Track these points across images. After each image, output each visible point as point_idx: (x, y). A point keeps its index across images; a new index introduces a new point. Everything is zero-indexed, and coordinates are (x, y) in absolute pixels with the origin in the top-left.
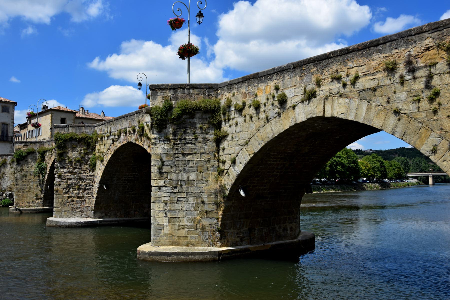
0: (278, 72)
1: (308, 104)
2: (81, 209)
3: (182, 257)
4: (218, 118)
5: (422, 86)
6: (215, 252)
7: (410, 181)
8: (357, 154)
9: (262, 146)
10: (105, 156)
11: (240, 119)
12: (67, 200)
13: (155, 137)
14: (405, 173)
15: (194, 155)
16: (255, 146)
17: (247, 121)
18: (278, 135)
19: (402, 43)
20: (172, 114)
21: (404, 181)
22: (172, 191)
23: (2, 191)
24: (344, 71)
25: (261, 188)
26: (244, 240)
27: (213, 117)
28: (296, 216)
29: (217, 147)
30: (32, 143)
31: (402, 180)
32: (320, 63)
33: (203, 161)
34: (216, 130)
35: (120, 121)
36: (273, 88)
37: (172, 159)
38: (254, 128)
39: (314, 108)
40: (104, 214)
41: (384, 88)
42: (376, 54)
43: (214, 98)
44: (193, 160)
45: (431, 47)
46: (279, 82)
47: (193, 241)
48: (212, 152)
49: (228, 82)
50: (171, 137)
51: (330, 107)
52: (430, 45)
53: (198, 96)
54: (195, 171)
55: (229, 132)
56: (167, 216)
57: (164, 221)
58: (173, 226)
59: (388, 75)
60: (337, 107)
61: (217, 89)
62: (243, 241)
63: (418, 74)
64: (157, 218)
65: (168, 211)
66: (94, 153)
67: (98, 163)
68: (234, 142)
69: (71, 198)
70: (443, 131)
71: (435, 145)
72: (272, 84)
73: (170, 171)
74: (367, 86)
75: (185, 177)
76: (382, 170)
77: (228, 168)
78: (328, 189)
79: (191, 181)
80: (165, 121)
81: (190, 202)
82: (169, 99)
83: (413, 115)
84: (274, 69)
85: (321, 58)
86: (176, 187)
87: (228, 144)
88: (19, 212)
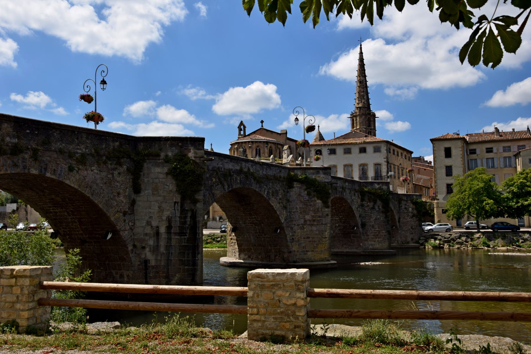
40: (247, 256)
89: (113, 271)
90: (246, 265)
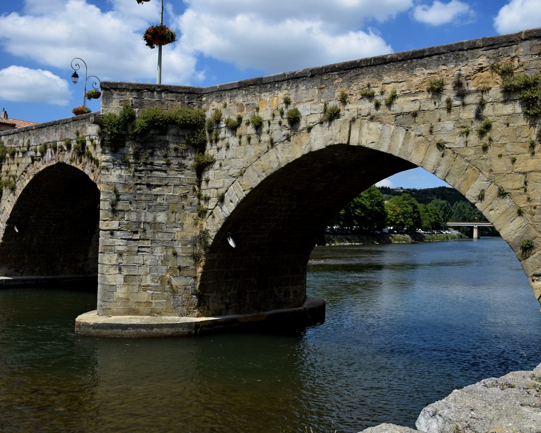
0: (289, 79)
1: (329, 127)
3: (143, 330)
4: (201, 137)
5: (472, 115)
7: (450, 233)
8: (383, 193)
9: (263, 179)
10: (17, 182)
11: (233, 141)
13: (107, 158)
14: (444, 222)
15: (165, 187)
16: (252, 179)
17: (242, 144)
18: (286, 166)
19: (451, 59)
20: (133, 127)
21: (442, 233)
22: (131, 237)
24: (378, 87)
26: (231, 308)
27: (194, 135)
28: (302, 276)
29: (197, 177)
31: (440, 232)
32: (347, 73)
34: (198, 153)
35: (45, 130)
36: (282, 101)
37: (131, 191)
38: (253, 154)
39: (337, 132)
40: (13, 270)
41: (427, 114)
42: (419, 69)
43: (196, 108)
44: (162, 194)
45: (485, 67)
46: (290, 93)
47: (159, 308)
48: (191, 184)
49: (218, 87)
50: (131, 160)
51: (358, 132)
52: (484, 66)
53: (173, 104)
54: (165, 210)
55: (216, 157)
56: (122, 273)
57: (117, 280)
58: (131, 287)
59: (433, 97)
61: (202, 96)
63: (469, 99)
64: (106, 276)
65: (124, 265)
67: (6, 192)
68: (224, 172)
70: (492, 173)
71: (483, 190)
72: (281, 95)
73: (128, 209)
74: (406, 110)
75: (150, 219)
76: (415, 217)
77: (212, 208)
78: (341, 240)
79: (160, 223)
80: (123, 136)
81: (156, 254)
82: (130, 105)
83: (459, 150)
84: (284, 75)
86: (136, 232)
87: (213, 174)
90: (18, 283)
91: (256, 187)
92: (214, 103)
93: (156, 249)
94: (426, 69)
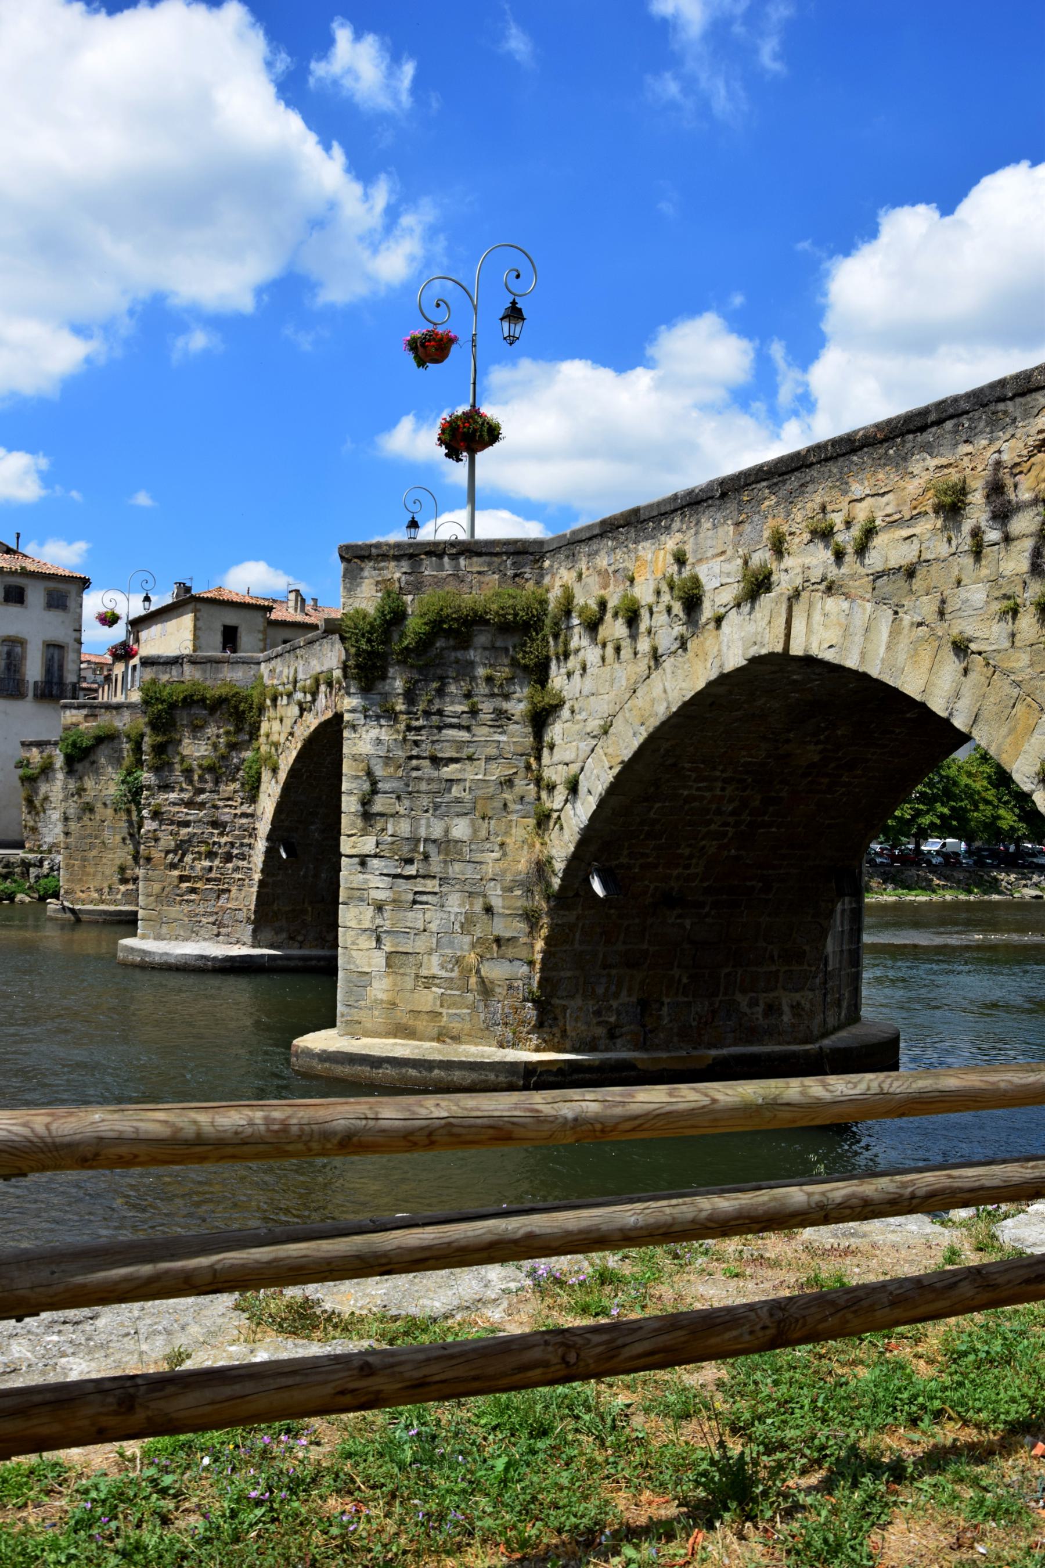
1: (750, 614)
2: (215, 917)
3: (412, 1072)
5: (1024, 566)
6: (514, 1064)
9: (641, 739)
11: (592, 654)
12: (177, 886)
17: (608, 661)
18: (680, 709)
19: (982, 424)
20: (403, 635)
22: (399, 870)
23: (41, 852)
25: (675, 873)
26: (621, 1035)
27: (524, 645)
28: (813, 969)
30: (108, 707)
32: (784, 482)
33: (491, 784)
37: (400, 773)
38: (624, 683)
40: (284, 935)
41: (934, 568)
43: (530, 585)
47: (456, 1026)
48: (522, 755)
50: (400, 707)
51: (804, 623)
57: (374, 961)
60: (819, 624)
61: (542, 558)
62: (617, 1038)
65: (386, 932)
66: (255, 745)
67: (266, 775)
69: (189, 881)
72: (670, 543)
73: (393, 811)
74: (893, 563)
75: (437, 832)
77: (559, 807)
79: (457, 842)
81: (449, 909)
83: (998, 657)
84: (675, 497)
85: (787, 466)
86: (410, 861)
88: (72, 918)
89: (739, 997)
90: (292, 964)
91: (630, 760)
92: (563, 571)
93: (450, 898)
94: (932, 457)
